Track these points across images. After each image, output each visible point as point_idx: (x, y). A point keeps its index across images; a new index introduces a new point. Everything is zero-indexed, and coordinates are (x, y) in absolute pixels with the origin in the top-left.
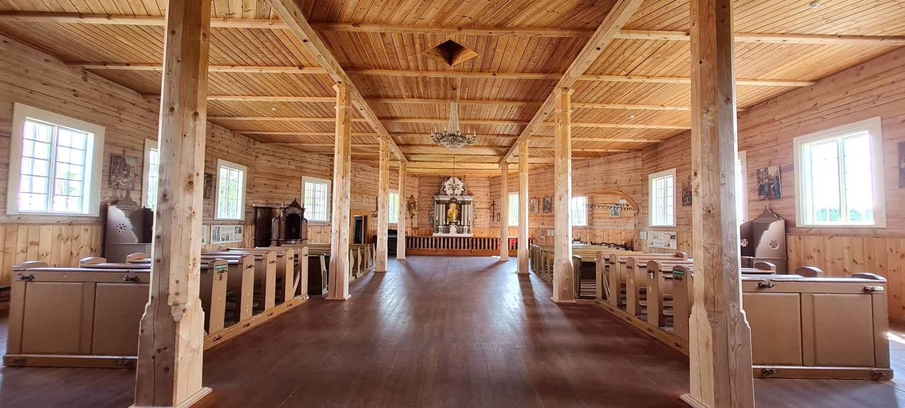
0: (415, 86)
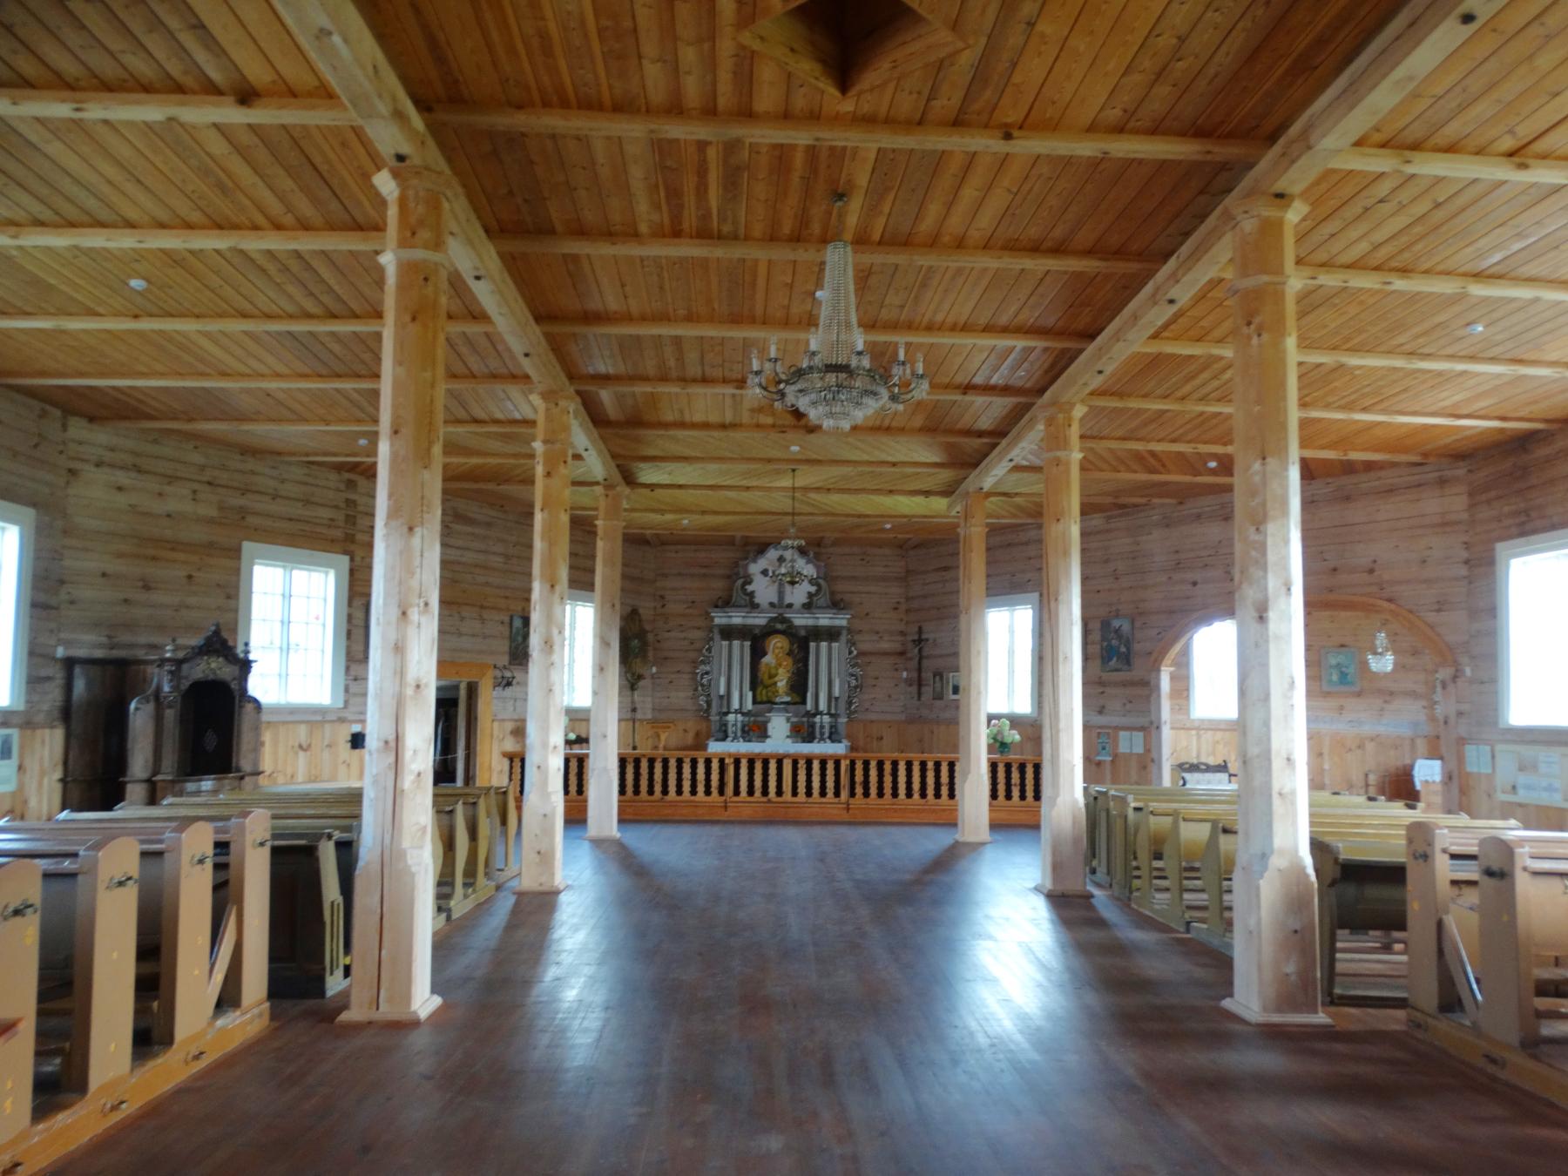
0: (689, 183)
